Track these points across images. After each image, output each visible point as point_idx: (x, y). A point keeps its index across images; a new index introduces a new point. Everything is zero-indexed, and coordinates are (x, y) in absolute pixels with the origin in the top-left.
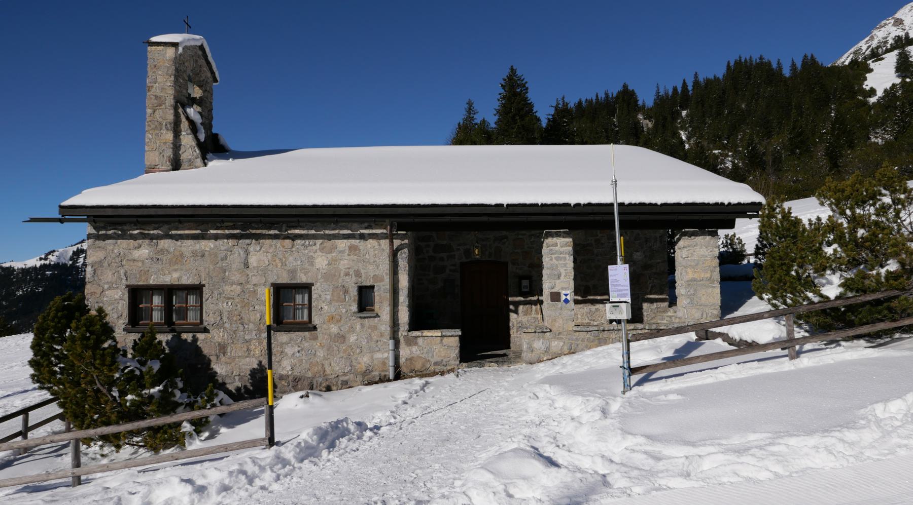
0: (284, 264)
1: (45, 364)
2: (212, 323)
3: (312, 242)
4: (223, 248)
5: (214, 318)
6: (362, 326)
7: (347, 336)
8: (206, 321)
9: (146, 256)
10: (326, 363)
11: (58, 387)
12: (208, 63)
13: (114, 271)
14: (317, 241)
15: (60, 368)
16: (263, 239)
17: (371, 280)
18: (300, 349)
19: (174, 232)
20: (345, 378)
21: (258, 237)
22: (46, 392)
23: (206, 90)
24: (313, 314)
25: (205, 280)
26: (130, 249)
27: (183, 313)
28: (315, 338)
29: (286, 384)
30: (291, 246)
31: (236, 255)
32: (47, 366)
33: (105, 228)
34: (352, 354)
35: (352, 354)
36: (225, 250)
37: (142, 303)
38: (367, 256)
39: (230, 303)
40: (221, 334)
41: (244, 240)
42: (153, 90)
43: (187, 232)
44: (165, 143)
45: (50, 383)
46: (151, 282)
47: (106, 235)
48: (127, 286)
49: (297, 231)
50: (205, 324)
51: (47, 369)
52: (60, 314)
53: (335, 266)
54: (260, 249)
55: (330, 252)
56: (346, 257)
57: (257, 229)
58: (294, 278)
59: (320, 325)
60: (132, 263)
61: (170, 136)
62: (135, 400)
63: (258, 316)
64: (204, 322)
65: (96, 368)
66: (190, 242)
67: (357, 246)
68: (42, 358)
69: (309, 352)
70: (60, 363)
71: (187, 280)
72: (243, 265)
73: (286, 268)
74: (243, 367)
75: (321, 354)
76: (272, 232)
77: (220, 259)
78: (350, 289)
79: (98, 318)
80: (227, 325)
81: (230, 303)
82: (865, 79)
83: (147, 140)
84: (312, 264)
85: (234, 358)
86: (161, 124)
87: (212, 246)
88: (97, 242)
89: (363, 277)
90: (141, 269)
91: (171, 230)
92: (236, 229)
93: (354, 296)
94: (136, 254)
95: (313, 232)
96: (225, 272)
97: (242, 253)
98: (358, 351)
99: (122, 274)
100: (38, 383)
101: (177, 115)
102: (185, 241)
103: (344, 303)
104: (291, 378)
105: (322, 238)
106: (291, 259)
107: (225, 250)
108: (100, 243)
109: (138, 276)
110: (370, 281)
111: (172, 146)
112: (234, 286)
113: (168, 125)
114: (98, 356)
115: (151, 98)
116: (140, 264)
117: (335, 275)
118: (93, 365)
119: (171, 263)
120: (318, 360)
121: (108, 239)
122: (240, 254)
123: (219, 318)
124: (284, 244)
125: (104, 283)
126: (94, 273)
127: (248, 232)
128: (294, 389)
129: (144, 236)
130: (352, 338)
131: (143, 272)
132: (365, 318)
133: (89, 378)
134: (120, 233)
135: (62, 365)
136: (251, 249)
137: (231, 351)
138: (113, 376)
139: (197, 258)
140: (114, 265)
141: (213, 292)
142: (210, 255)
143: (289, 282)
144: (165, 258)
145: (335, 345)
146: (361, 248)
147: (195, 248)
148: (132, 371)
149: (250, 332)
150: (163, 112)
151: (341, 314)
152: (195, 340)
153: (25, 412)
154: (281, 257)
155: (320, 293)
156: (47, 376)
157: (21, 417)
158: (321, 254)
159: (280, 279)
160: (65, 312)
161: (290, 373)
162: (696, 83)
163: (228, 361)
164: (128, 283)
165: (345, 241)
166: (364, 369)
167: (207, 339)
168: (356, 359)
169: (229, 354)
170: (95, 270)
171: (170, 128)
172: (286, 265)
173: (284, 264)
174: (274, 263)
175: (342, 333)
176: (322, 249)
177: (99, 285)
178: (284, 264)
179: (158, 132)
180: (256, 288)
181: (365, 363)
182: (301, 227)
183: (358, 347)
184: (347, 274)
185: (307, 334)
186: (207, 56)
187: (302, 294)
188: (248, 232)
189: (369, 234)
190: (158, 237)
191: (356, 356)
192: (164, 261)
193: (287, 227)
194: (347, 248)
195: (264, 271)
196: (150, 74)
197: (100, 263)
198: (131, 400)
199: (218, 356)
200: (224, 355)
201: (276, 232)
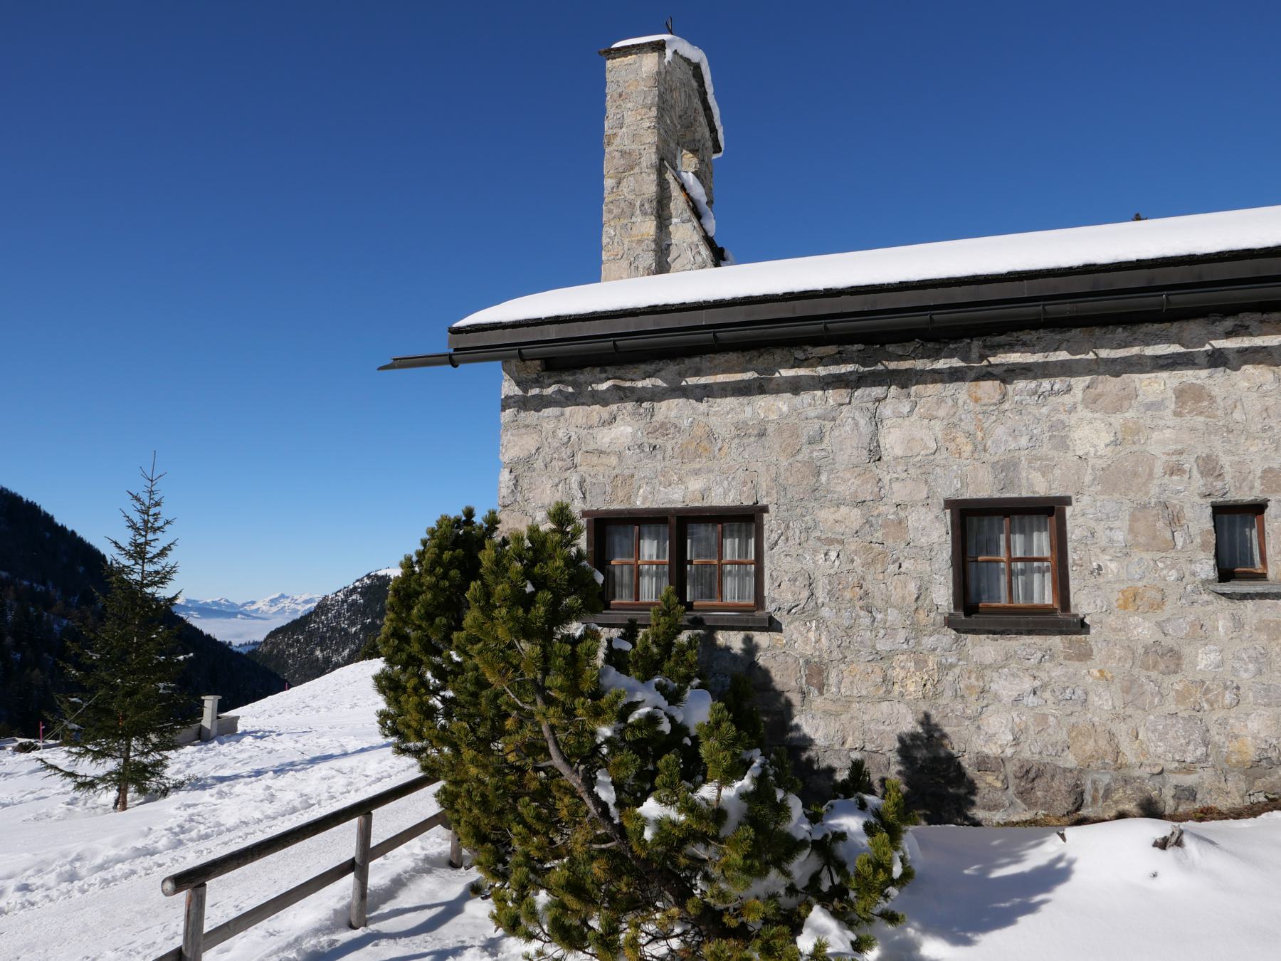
0: (980, 448)
1: (410, 685)
2: (787, 606)
3: (1059, 384)
4: (812, 414)
5: (794, 594)
6: (1238, 624)
7: (1186, 650)
8: (774, 600)
9: (628, 441)
10: (1121, 730)
11: (440, 751)
12: (707, 109)
13: (557, 480)
14: (1073, 381)
15: (444, 700)
16: (917, 383)
17: (1257, 483)
18: (1037, 683)
19: (692, 381)
20: (1189, 780)
21: (905, 380)
22: (414, 761)
23: (703, 161)
24: (1074, 585)
25: (768, 494)
26: (591, 427)
27: (714, 586)
28: (1085, 655)
29: (999, 784)
30: (998, 397)
31: (848, 428)
32: (415, 689)
33: (538, 382)
34: (1206, 706)
35: (1206, 706)
36: (818, 418)
37: (613, 558)
38: (1238, 415)
39: (833, 555)
40: (812, 636)
41: (868, 390)
42: (617, 141)
43: (721, 378)
44: (640, 242)
45: (421, 738)
47: (539, 397)
49: (1015, 358)
50: (770, 607)
51: (414, 699)
52: (447, 555)
53: (1135, 448)
54: (911, 411)
55: (1118, 409)
56: (1170, 420)
57: (901, 358)
58: (1011, 483)
59: (1096, 618)
60: (595, 460)
61: (649, 227)
62: (673, 824)
63: (912, 588)
64: (767, 603)
65: (549, 701)
66: (730, 402)
67: (1203, 388)
68: (404, 669)
69: (1068, 694)
70: (444, 689)
71: (724, 496)
72: (865, 452)
73: (987, 457)
74: (872, 726)
75: (1104, 702)
76: (942, 364)
77: (804, 439)
78: (1188, 513)
79: (557, 537)
80: (825, 612)
81: (833, 555)
83: (605, 240)
84: (1063, 444)
85: (848, 702)
86: (631, 205)
87: (785, 409)
88: (522, 414)
89: (1228, 478)
90: (617, 471)
91: (683, 375)
92: (845, 362)
93: (1202, 533)
94: (605, 437)
95: (1062, 355)
96: (819, 473)
97: (862, 422)
98: (1228, 697)
99: (575, 486)
100: (393, 735)
101: (662, 185)
102: (718, 400)
103: (1172, 554)
104: (1011, 768)
105: (1089, 372)
106: (1000, 431)
107: (818, 418)
108: (530, 417)
109: (608, 489)
110: (1252, 488)
111: (653, 246)
112: (843, 509)
113: (647, 206)
114: (560, 662)
115: (613, 158)
116: (613, 460)
117: (1135, 474)
118: (541, 689)
119: (684, 455)
120: (1096, 719)
121: (546, 407)
122: (857, 424)
123: (806, 594)
124: (980, 393)
125: (535, 508)
126: (515, 486)
127: (880, 367)
128: (1024, 801)
129: (622, 395)
130: (1204, 660)
131: (620, 478)
132: (1244, 597)
133: (527, 733)
134: (570, 390)
135: (449, 694)
136: (887, 410)
137: (840, 683)
138: (593, 734)
139: (746, 441)
140: (557, 464)
141: (788, 527)
142: (780, 431)
143: (997, 495)
144: (669, 445)
145: (1148, 677)
146: (1216, 391)
147: (742, 417)
148: (652, 720)
149: (890, 631)
150: (637, 181)
151: (1161, 585)
152: (751, 648)
153: (364, 809)
154: (972, 428)
155: (1093, 524)
156: (413, 718)
157: (354, 823)
158: (1090, 415)
159: (971, 487)
160: (460, 552)
161: (1009, 752)
163: (831, 707)
164: (587, 507)
165: (1164, 375)
166: (1252, 755)
167: (774, 647)
168: (1223, 723)
169: (834, 689)
170: (517, 479)
171: (649, 211)
172: (985, 450)
173: (980, 448)
174: (952, 446)
175: (1168, 642)
176: (1092, 402)
177: (525, 513)
178: (980, 448)
179: (626, 222)
180: (902, 514)
181: (1255, 738)
182: (1024, 344)
183: (1226, 688)
184: (1175, 470)
185: (1056, 641)
186: (705, 93)
187: (1022, 531)
188: (880, 367)
189: (1242, 352)
190: (656, 396)
191: (1219, 714)
192: (669, 452)
193: (985, 347)
194: (1170, 394)
195: (925, 469)
196: (611, 110)
197: (528, 461)
198: (659, 823)
199: (804, 694)
200: (821, 693)
201: (956, 362)
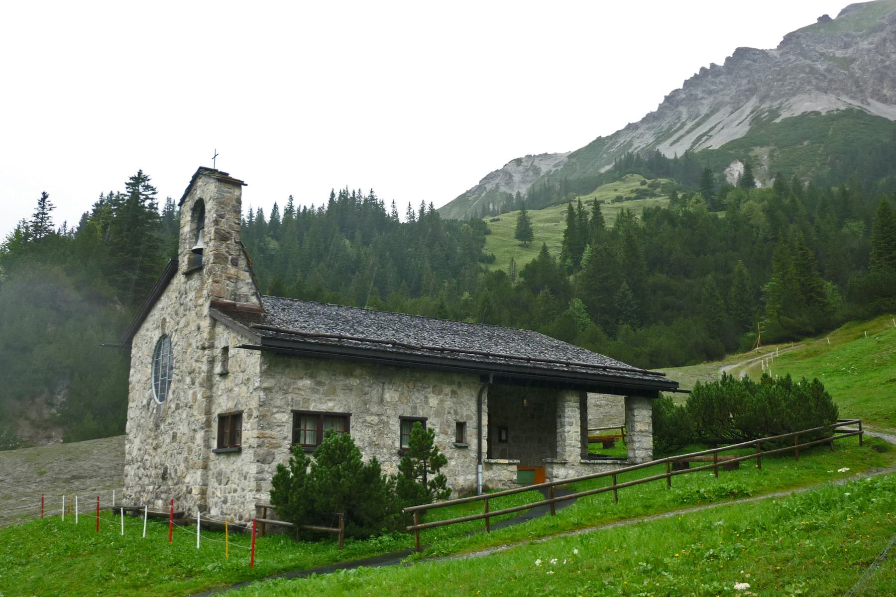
46: (311, 409)
48: (292, 411)
82: (403, 223)
162: (289, 211)
166: (460, 487)
